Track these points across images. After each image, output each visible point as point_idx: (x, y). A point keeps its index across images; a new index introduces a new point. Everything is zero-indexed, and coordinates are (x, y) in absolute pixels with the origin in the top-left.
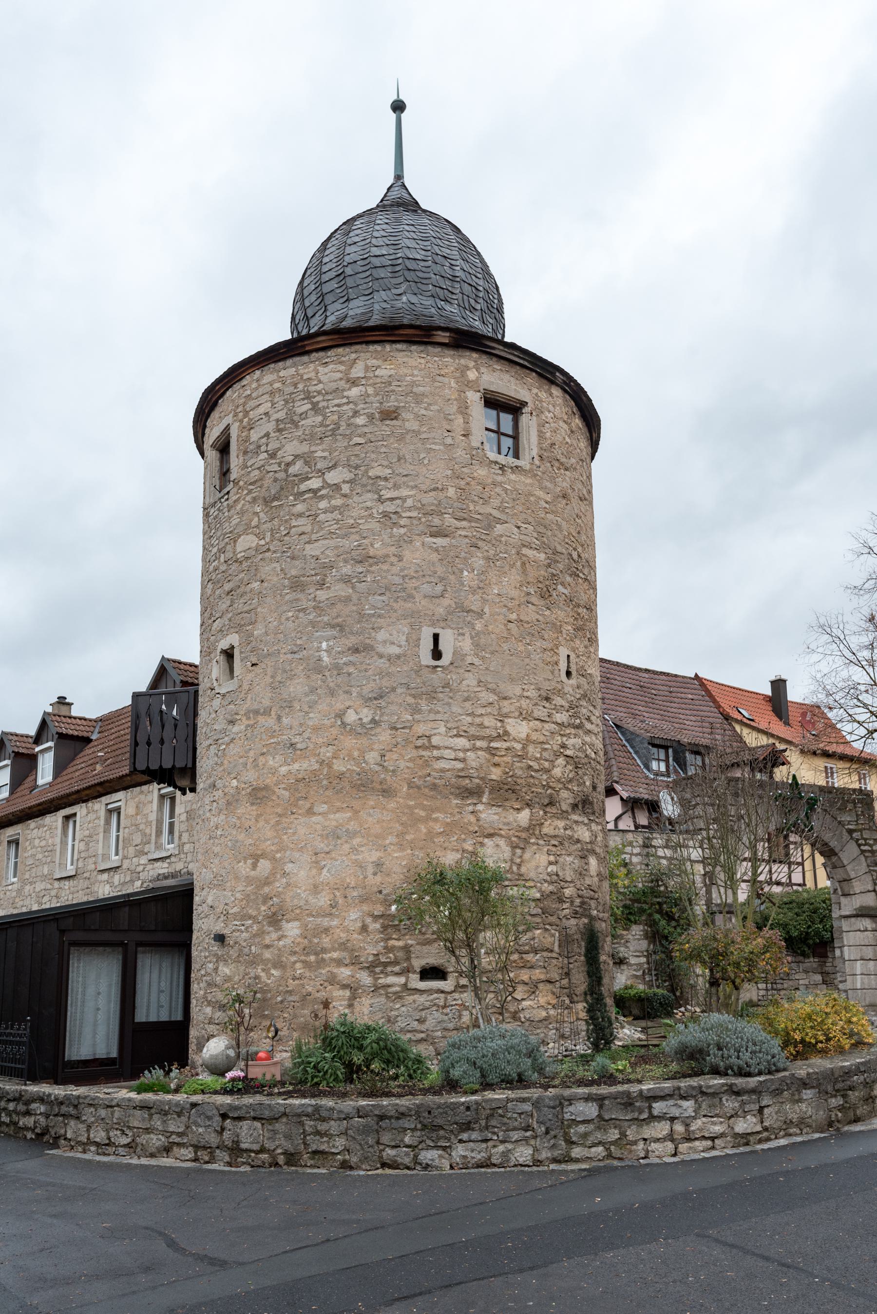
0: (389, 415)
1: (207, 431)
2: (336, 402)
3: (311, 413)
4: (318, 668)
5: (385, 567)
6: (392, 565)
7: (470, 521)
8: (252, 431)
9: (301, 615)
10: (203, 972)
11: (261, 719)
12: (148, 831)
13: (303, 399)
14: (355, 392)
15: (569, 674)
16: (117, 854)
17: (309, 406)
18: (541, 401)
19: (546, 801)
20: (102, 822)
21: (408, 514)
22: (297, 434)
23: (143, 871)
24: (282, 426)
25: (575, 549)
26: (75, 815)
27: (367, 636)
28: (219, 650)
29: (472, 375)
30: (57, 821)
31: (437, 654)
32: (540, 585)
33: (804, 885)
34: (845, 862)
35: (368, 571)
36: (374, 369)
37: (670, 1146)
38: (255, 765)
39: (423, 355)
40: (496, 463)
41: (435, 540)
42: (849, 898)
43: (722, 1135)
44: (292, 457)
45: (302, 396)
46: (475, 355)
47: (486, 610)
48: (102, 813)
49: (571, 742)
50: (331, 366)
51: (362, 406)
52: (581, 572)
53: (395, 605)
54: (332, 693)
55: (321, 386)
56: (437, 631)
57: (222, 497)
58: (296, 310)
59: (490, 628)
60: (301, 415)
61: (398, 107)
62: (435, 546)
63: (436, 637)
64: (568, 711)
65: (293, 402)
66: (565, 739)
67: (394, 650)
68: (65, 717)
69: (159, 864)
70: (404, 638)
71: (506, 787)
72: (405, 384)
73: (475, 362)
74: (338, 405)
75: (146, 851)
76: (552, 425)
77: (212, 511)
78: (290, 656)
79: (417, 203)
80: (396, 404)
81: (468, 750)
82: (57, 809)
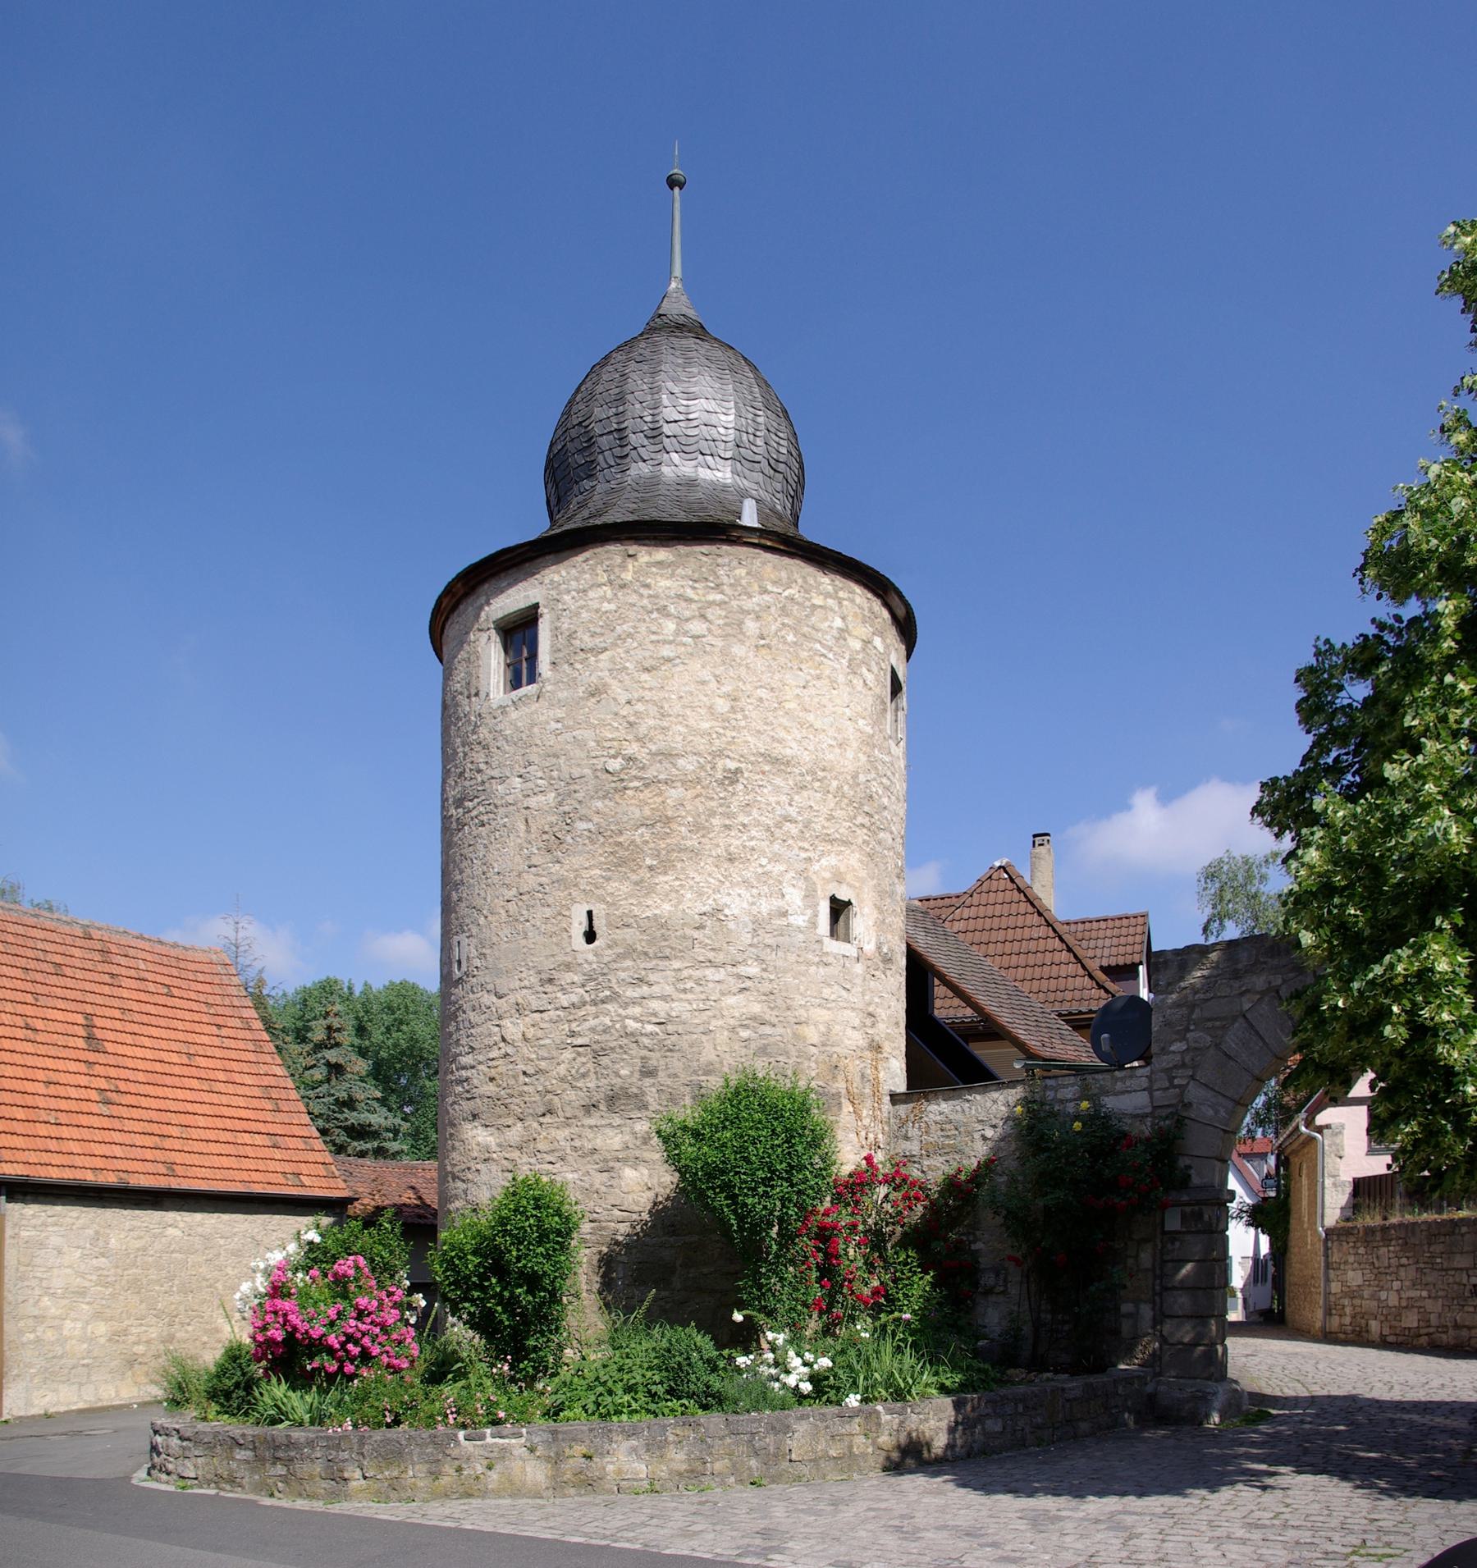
15: (590, 936)
19: (542, 1110)
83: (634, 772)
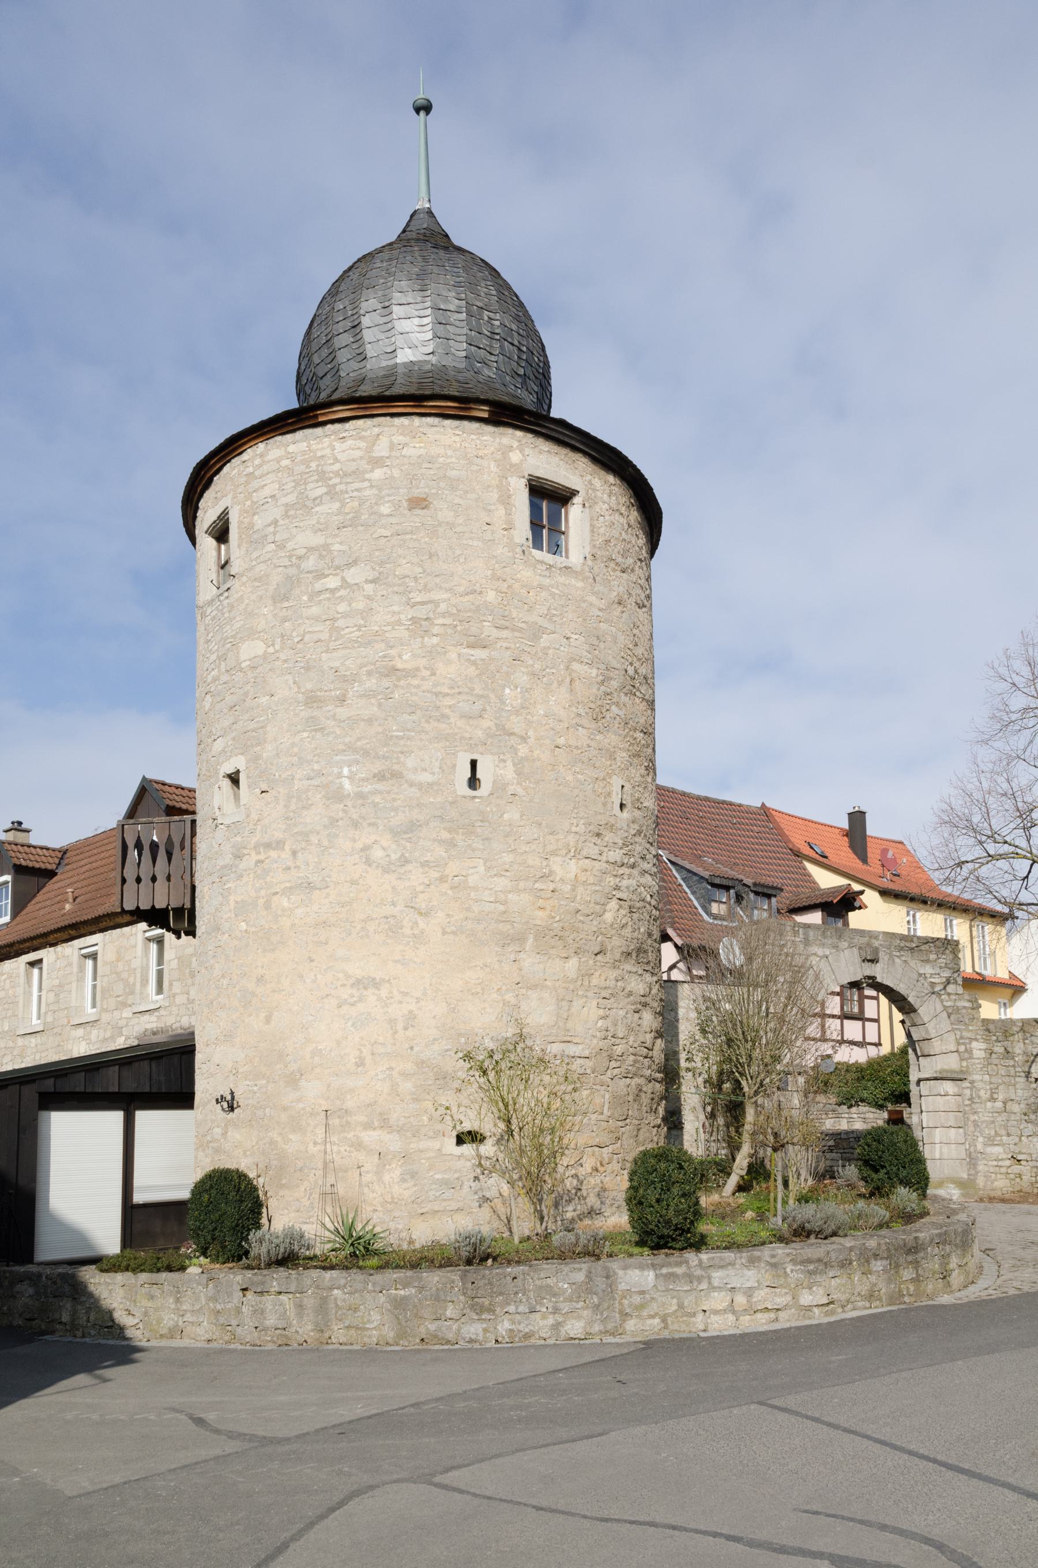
0: (419, 503)
1: (199, 514)
2: (356, 485)
3: (326, 498)
4: (339, 796)
5: (415, 682)
6: (423, 679)
7: (513, 630)
8: (256, 517)
9: (318, 735)
10: (209, 1138)
11: (273, 854)
12: (131, 980)
13: (317, 481)
14: (378, 474)
16: (94, 1006)
17: (324, 490)
18: (594, 490)
19: (597, 950)
20: (75, 970)
21: (440, 621)
22: (309, 522)
23: (126, 1026)
24: (292, 512)
25: (631, 664)
26: (40, 961)
27: (394, 761)
28: (222, 774)
29: (515, 457)
30: (19, 968)
31: (473, 782)
32: (593, 706)
33: (880, 1044)
34: (926, 1020)
35: (396, 686)
36: (401, 447)
37: (731, 1317)
38: (267, 906)
39: (457, 432)
40: (542, 562)
41: (472, 652)
42: (928, 1059)
43: (785, 1307)
44: (304, 551)
45: (316, 477)
46: (519, 433)
47: (531, 733)
48: (75, 958)
49: (625, 883)
50: (350, 442)
51: (387, 491)
52: (639, 690)
53: (426, 726)
54: (356, 825)
55: (337, 466)
56: (474, 758)
57: (221, 595)
58: (303, 368)
59: (536, 753)
60: (315, 499)
62: (473, 658)
63: (474, 764)
64: (621, 848)
65: (306, 484)
66: (618, 880)
67: (426, 777)
68: (22, 846)
69: (146, 1017)
70: (437, 764)
71: (552, 934)
72: (438, 466)
73: (519, 441)
74: (357, 490)
75: (129, 1002)
76: (607, 518)
77: (209, 610)
78: (306, 783)
79: (447, 236)
80: (427, 490)
81: (510, 892)
82: (18, 954)
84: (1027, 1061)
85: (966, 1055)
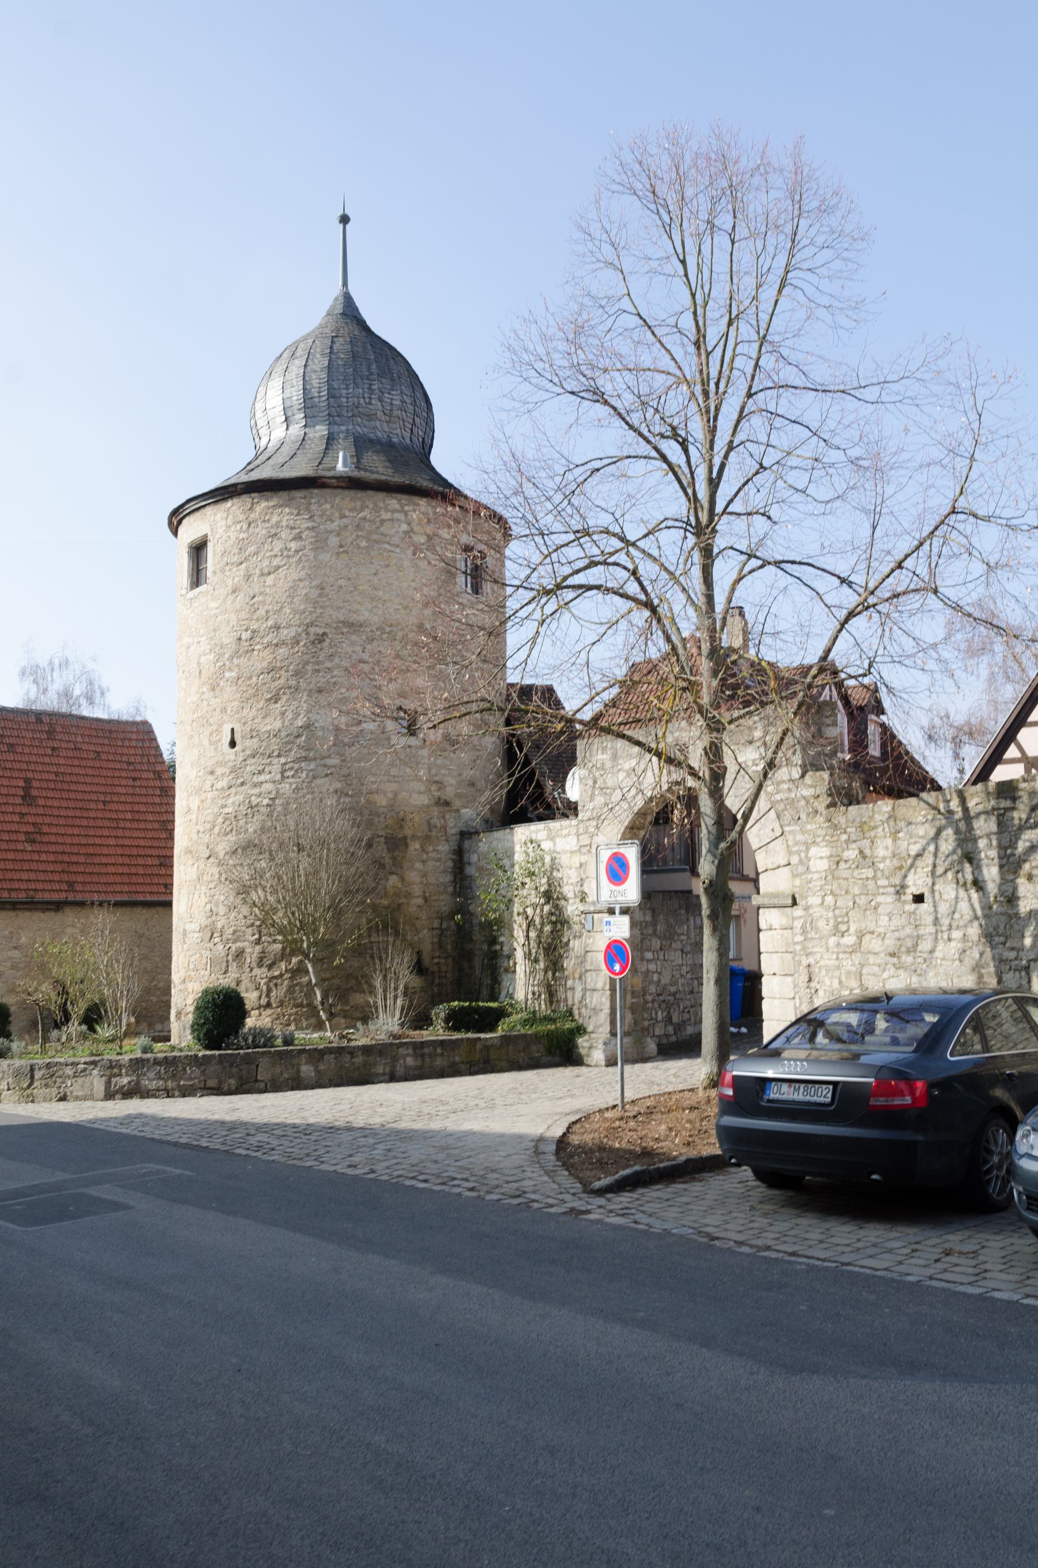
15: (233, 744)
61: (345, 220)
83: (258, 640)
84: (901, 868)
85: (801, 869)
